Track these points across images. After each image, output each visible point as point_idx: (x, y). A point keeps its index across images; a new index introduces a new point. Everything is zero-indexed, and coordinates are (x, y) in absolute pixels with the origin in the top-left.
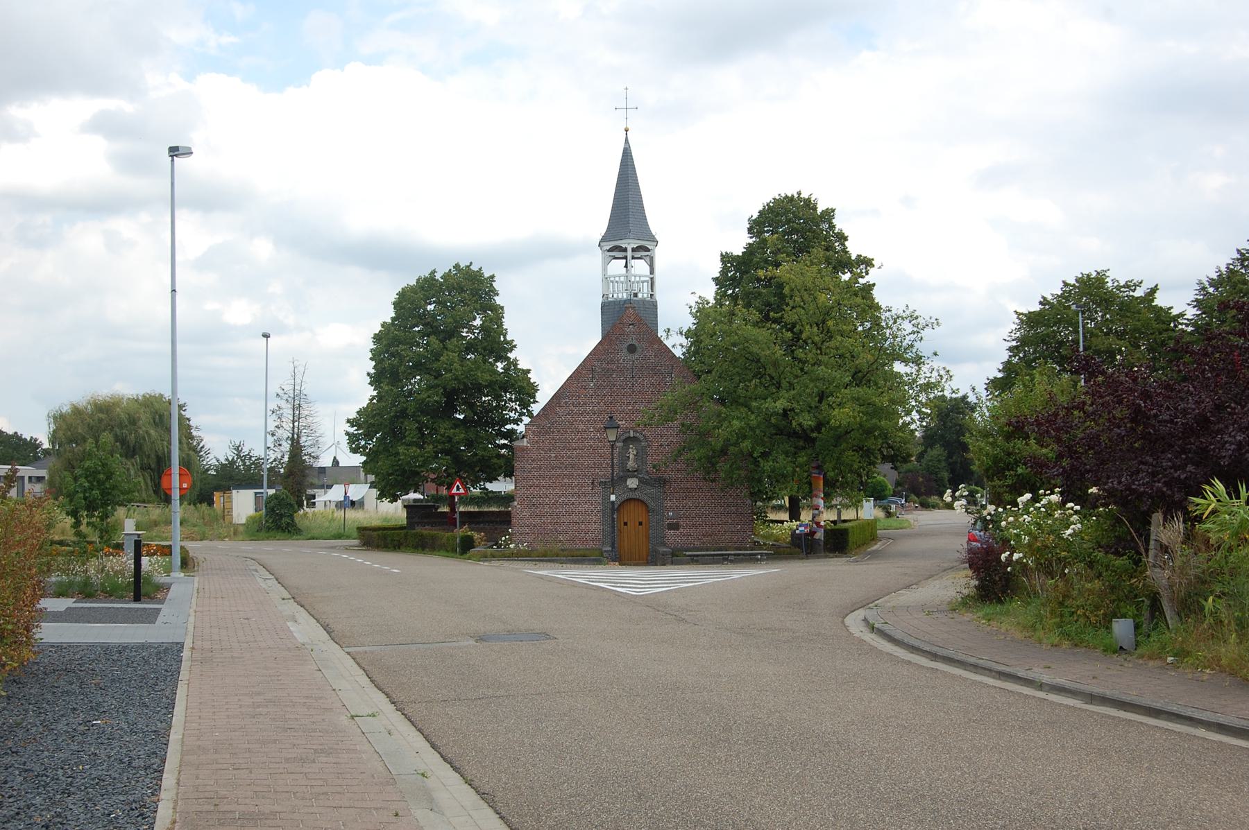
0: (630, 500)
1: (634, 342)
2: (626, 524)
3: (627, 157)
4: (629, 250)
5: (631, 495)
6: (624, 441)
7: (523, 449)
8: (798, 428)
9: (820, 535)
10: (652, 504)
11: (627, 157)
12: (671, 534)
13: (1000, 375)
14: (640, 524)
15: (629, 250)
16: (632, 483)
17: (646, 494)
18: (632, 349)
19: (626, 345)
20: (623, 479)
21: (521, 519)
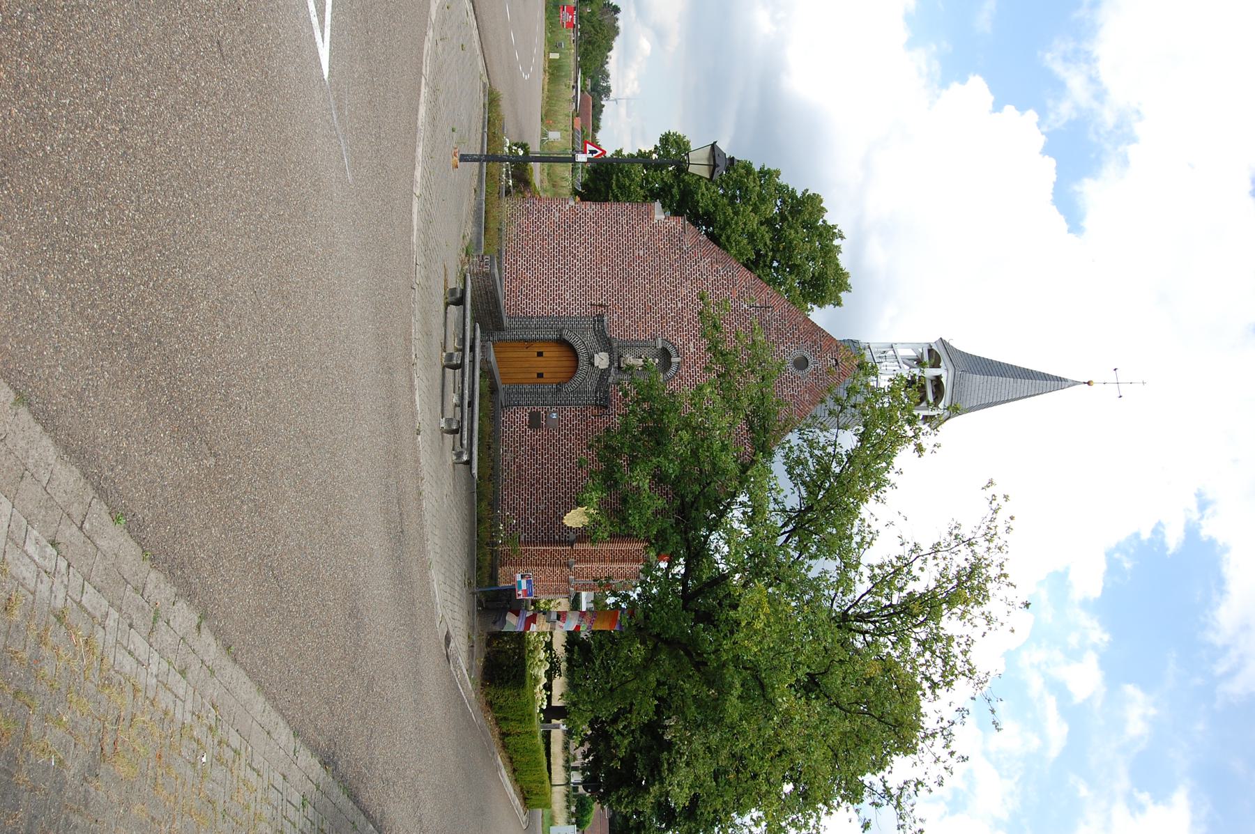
0: (577, 360)
1: (811, 367)
2: (540, 354)
3: (1054, 382)
4: (936, 372)
5: (583, 358)
6: (664, 350)
7: (649, 214)
8: (378, 815)
9: (513, 623)
10: (569, 387)
11: (1054, 382)
12: (523, 415)
13: (799, 195)
14: (540, 354)
15: (936, 372)
16: (602, 360)
17: (585, 381)
18: (801, 364)
19: (806, 354)
20: (607, 344)
21: (549, 211)
